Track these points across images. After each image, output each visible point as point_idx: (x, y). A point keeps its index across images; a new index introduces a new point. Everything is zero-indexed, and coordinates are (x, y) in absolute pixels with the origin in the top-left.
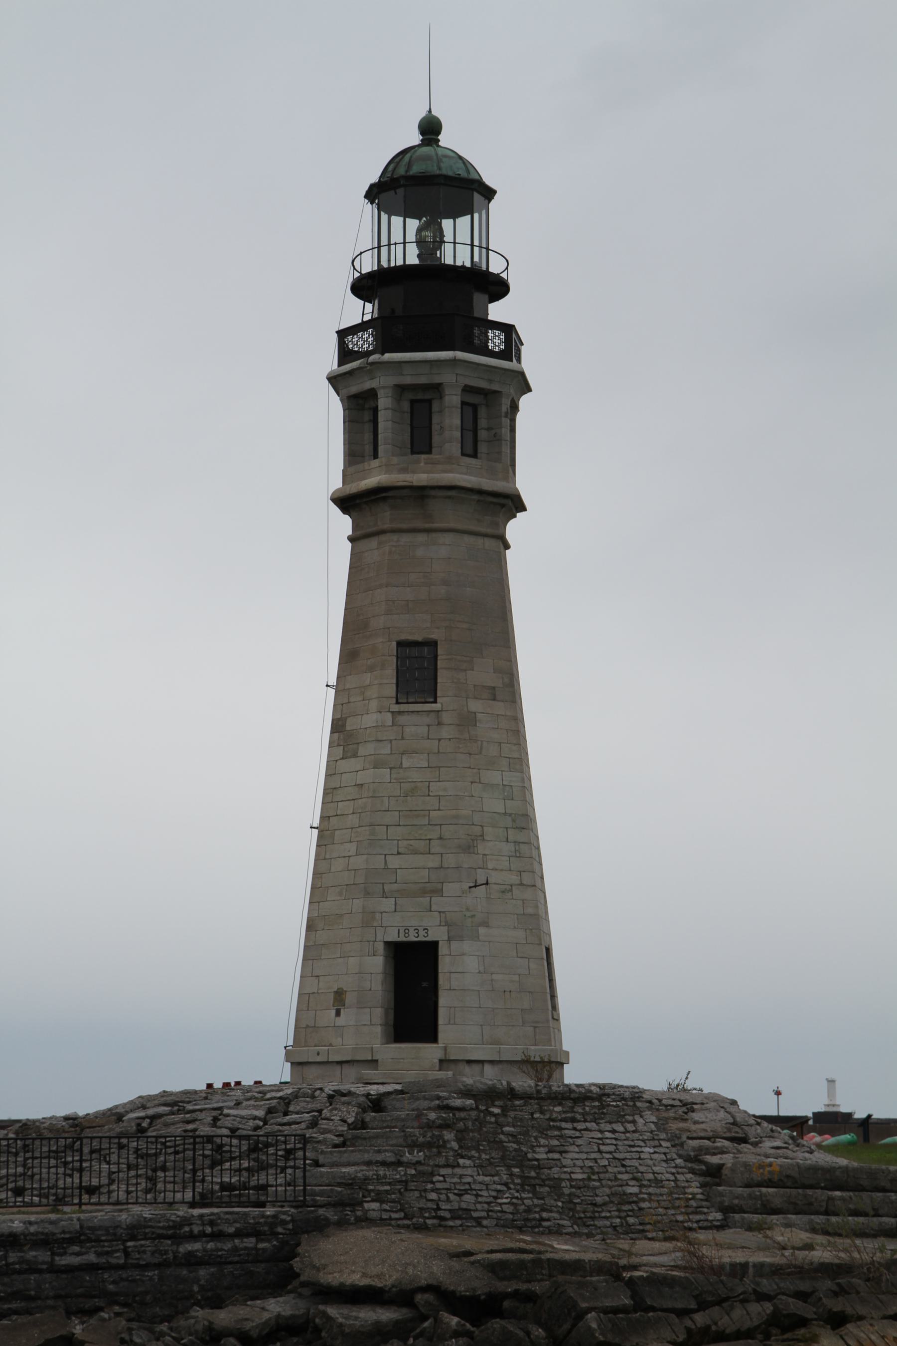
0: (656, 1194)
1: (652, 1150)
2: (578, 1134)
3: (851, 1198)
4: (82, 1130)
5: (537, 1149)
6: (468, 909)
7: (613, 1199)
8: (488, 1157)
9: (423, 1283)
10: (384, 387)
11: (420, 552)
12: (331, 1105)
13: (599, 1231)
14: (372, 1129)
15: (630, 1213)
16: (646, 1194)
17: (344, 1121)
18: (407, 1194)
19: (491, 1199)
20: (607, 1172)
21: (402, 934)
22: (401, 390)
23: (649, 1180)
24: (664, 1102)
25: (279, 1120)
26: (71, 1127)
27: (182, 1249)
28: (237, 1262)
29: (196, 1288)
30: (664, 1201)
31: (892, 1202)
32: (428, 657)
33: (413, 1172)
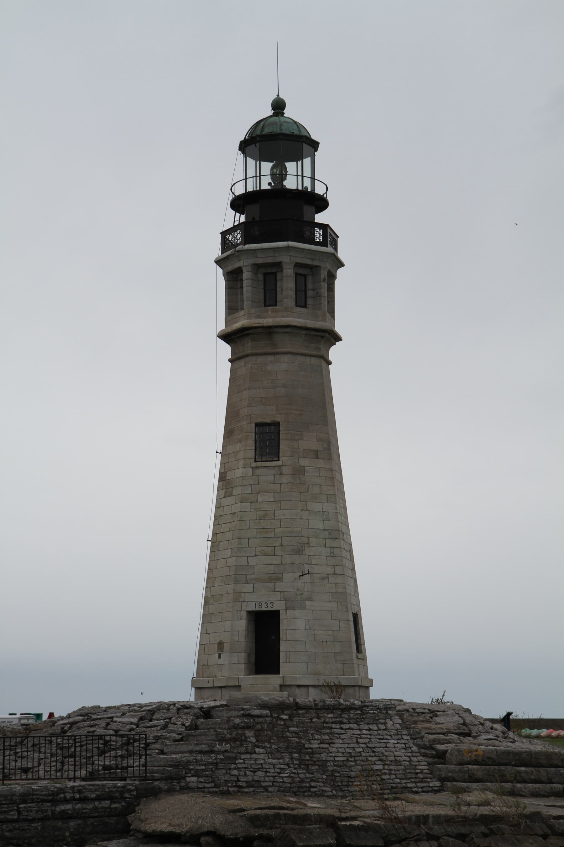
0: (395, 770)
1: (395, 742)
2: (343, 731)
3: (532, 772)
4: (30, 732)
5: (313, 742)
6: (298, 590)
8: (276, 747)
9: (205, 829)
11: (269, 367)
13: (351, 794)
14: (201, 729)
15: (375, 782)
16: (388, 770)
17: (183, 725)
19: (276, 774)
20: (361, 755)
21: (257, 606)
22: (257, 267)
23: (391, 761)
24: (417, 710)
27: (58, 809)
29: (67, 834)
30: (400, 774)
31: (561, 774)
32: (280, 434)
33: (222, 757)
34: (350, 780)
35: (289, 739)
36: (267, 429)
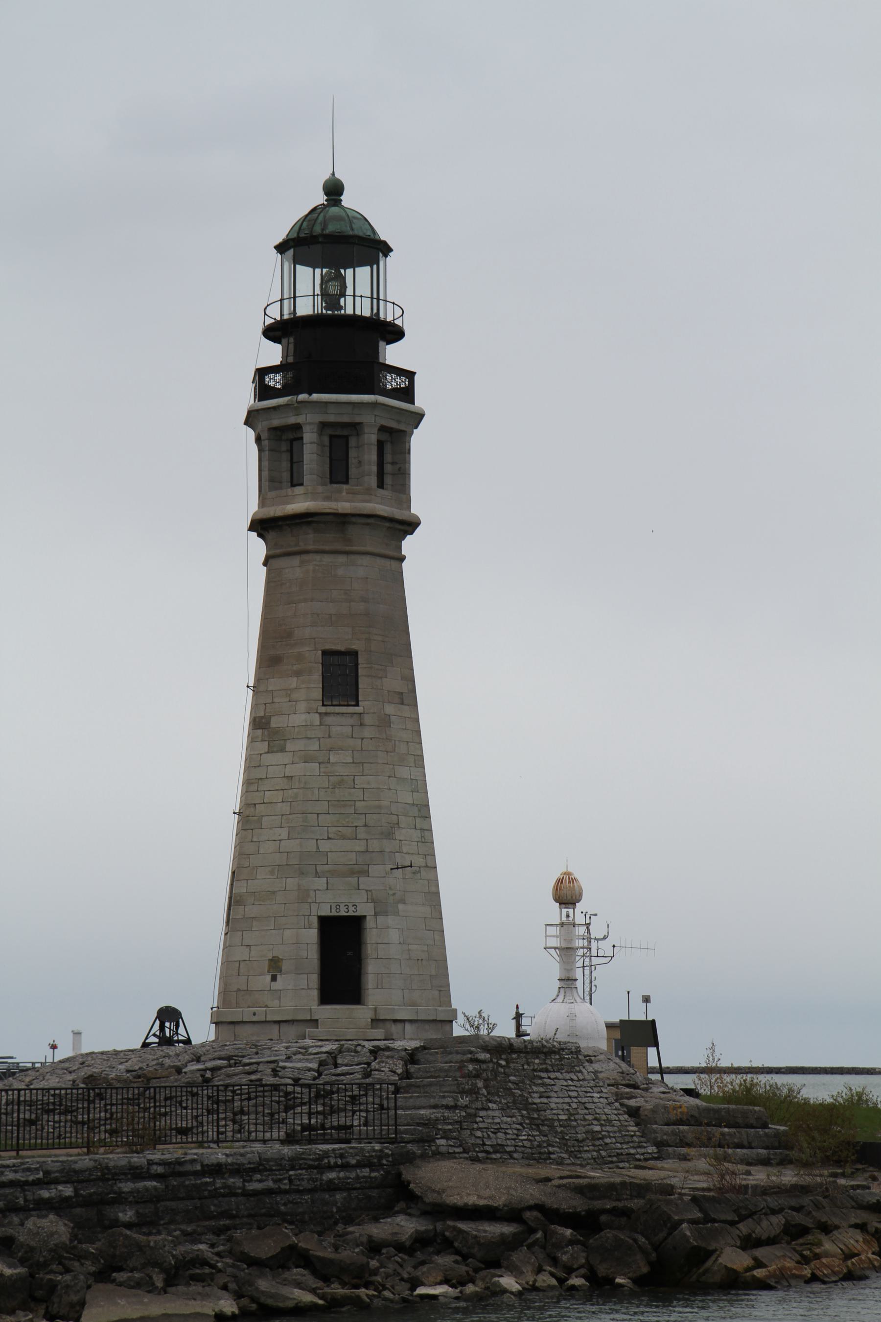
9: (532, 1202)
10: (310, 424)
11: (340, 572)
12: (375, 1059)
21: (334, 910)
22: (323, 425)
25: (333, 1071)
26: (135, 1078)
28: (359, 1189)
32: (335, 661)
33: (464, 1114)
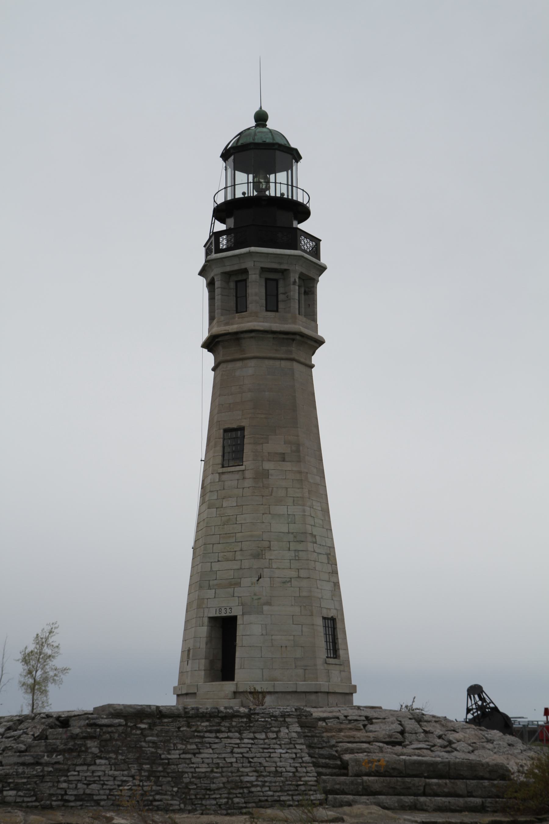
0: (271, 782)
2: (217, 741)
3: (446, 784)
6: (255, 595)
7: (227, 785)
8: (123, 758)
18: (41, 785)
21: (223, 611)
31: (485, 787)
34: (208, 792)
35: (143, 749)
36: (234, 434)
